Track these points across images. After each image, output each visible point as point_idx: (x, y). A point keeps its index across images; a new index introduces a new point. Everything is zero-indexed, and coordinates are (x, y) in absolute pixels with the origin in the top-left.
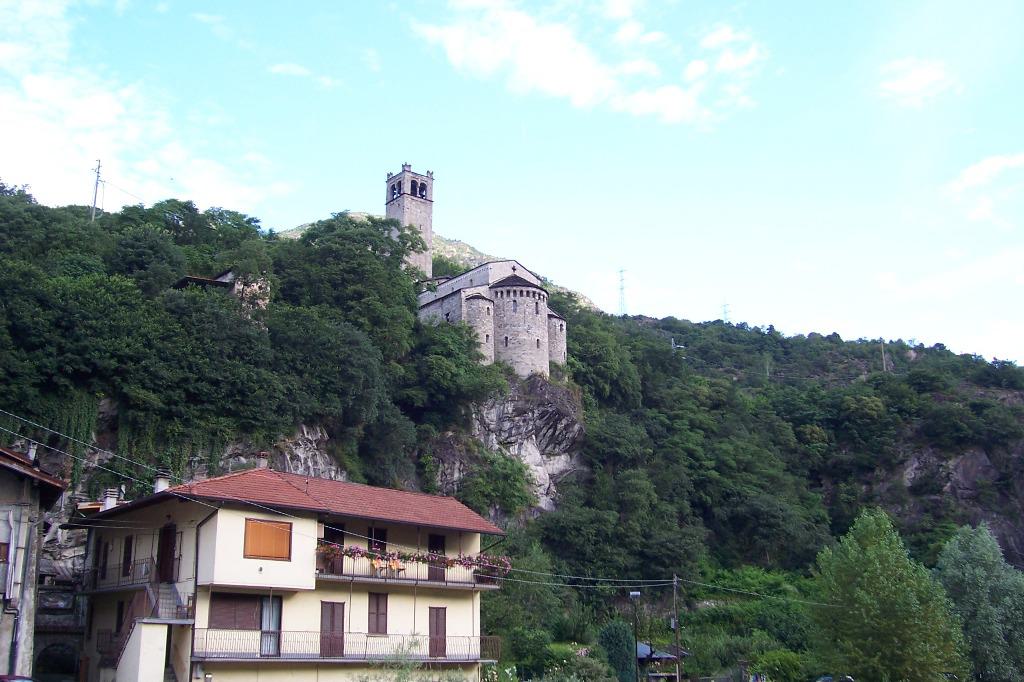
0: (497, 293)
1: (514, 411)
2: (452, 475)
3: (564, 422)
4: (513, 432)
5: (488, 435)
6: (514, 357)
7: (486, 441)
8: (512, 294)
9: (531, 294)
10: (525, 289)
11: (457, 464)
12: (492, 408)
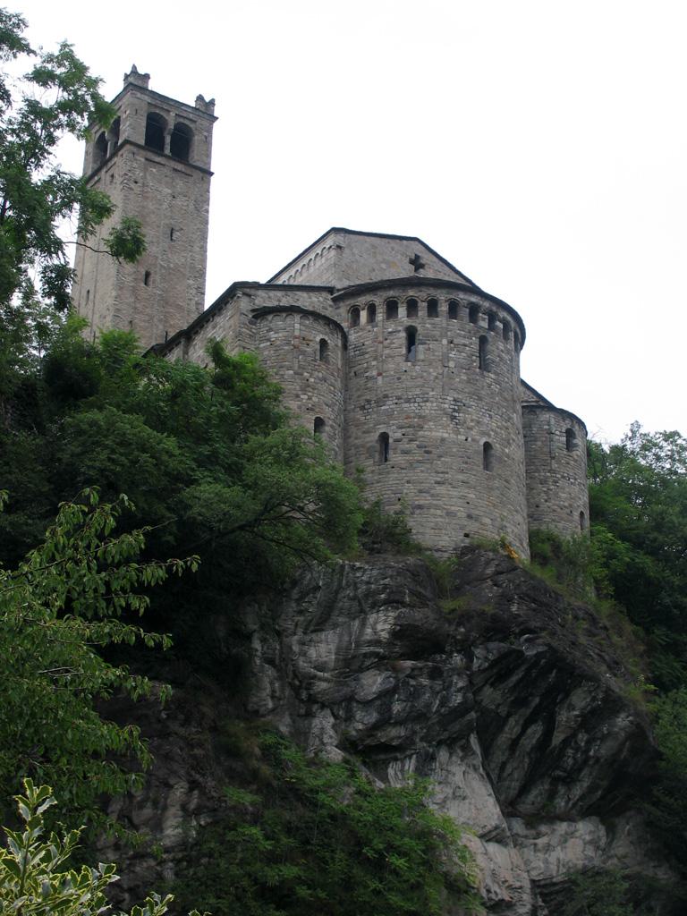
0: (355, 312)
1: (395, 635)
2: (157, 826)
3: (580, 700)
4: (397, 707)
5: (309, 715)
6: (409, 491)
7: (300, 736)
8: (402, 311)
9: (465, 312)
10: (442, 296)
11: (179, 791)
12: (319, 628)
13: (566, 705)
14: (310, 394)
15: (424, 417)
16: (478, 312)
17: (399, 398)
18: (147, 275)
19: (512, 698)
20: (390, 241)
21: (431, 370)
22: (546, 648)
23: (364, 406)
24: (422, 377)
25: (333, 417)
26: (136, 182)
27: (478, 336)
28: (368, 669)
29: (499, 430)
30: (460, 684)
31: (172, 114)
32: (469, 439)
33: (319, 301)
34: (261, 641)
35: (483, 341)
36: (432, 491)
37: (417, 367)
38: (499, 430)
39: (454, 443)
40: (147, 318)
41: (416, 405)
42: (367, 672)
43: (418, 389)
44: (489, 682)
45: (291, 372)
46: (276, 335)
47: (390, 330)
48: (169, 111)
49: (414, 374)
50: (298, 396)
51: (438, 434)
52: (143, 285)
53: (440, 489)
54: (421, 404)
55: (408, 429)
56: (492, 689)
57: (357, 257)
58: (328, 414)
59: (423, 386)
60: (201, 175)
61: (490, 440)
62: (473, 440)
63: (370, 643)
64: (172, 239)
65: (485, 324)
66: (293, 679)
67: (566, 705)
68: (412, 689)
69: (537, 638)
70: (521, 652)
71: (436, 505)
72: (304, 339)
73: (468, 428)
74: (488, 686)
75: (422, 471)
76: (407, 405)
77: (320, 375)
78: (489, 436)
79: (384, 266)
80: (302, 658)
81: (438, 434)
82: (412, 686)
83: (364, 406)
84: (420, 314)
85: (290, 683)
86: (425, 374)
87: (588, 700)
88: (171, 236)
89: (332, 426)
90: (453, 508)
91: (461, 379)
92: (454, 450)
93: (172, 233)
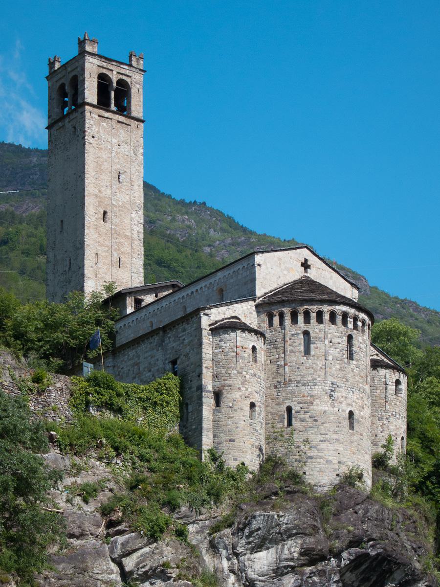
1: (301, 554)
8: (301, 318)
9: (339, 319)
13: (391, 579)
14: (247, 386)
15: (314, 396)
16: (348, 318)
17: (298, 382)
18: (105, 213)
19: (362, 577)
20: (289, 251)
21: (318, 363)
22: (382, 550)
23: (276, 386)
24: (312, 368)
25: (260, 400)
26: (93, 137)
27: (347, 335)
28: (286, 573)
29: (357, 401)
30: (336, 579)
31: (115, 73)
32: (340, 410)
33: (247, 309)
34: (227, 559)
35: (350, 338)
36: (318, 447)
37: (309, 360)
38: (357, 401)
39: (331, 413)
40: (106, 249)
41: (309, 387)
42: (286, 576)
43: (310, 376)
44: (350, 570)
45: (235, 372)
46: (225, 345)
47: (293, 333)
48: (112, 70)
49: (308, 365)
50: (239, 388)
51: (321, 408)
52: (102, 222)
53: (323, 446)
54: (312, 387)
55: (304, 405)
56: (350, 574)
57: (270, 270)
58: (257, 399)
59: (313, 374)
60: (137, 123)
61: (352, 409)
62: (343, 410)
63: (287, 560)
64: (119, 182)
65: (351, 326)
66: (245, 582)
67: (391, 579)
68: (310, 585)
69: (377, 544)
70: (369, 554)
71: (320, 456)
72: (242, 347)
73: (340, 402)
74: (349, 572)
75: (312, 434)
76: (303, 387)
77: (252, 372)
78: (352, 405)
79: (285, 272)
80: (250, 570)
81: (321, 408)
82: (310, 583)
83: (276, 386)
84: (312, 321)
85: (243, 584)
86: (314, 365)
87: (403, 575)
88: (119, 179)
89: (259, 406)
90: (330, 458)
91: (336, 368)
92: (332, 418)
93: (119, 176)
